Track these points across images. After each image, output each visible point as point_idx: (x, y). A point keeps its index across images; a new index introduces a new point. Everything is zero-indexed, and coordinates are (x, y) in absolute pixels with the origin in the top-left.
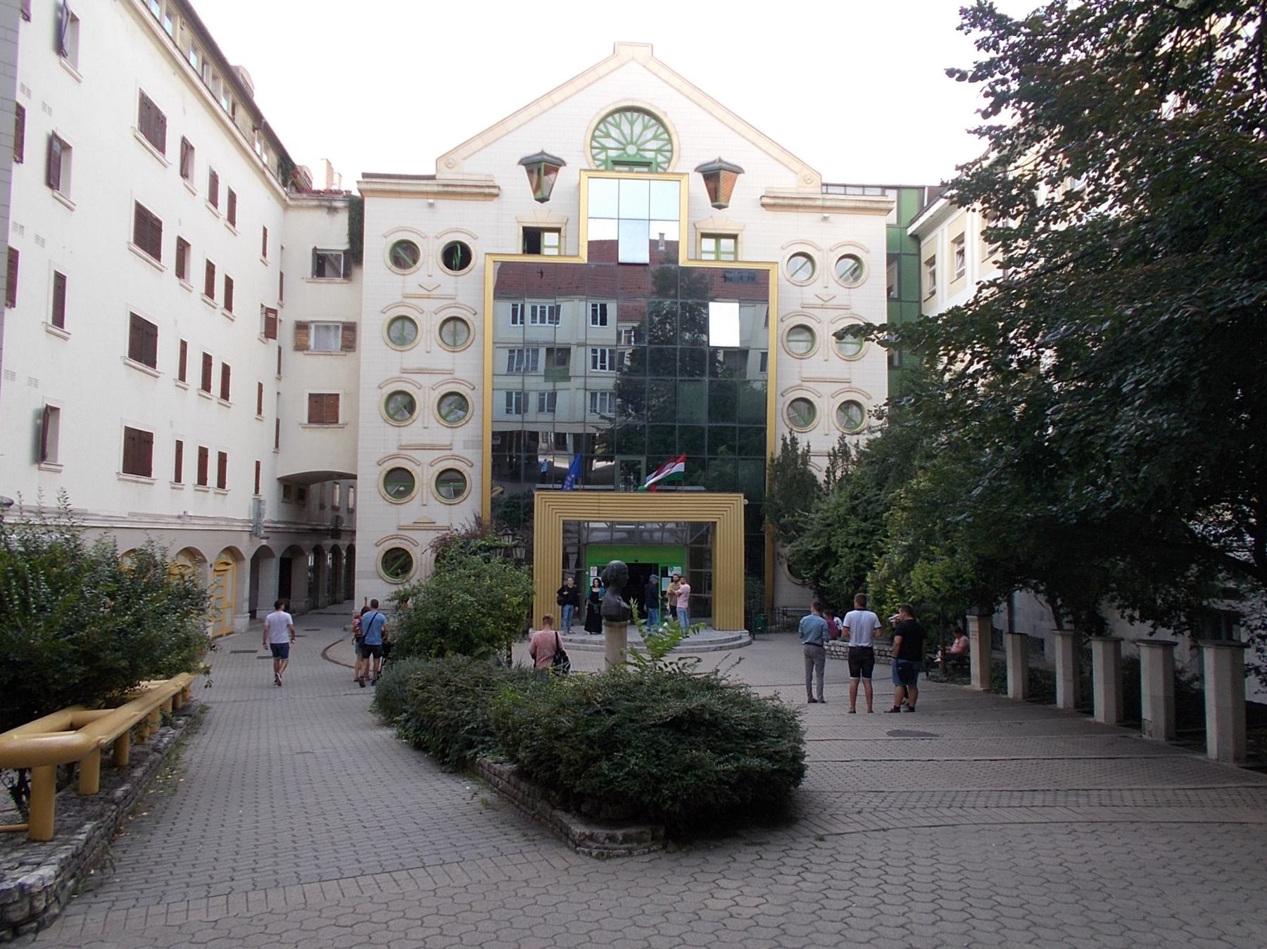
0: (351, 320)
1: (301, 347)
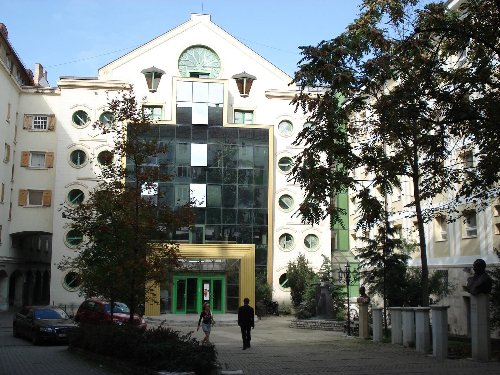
0: (50, 189)
1: (24, 165)
